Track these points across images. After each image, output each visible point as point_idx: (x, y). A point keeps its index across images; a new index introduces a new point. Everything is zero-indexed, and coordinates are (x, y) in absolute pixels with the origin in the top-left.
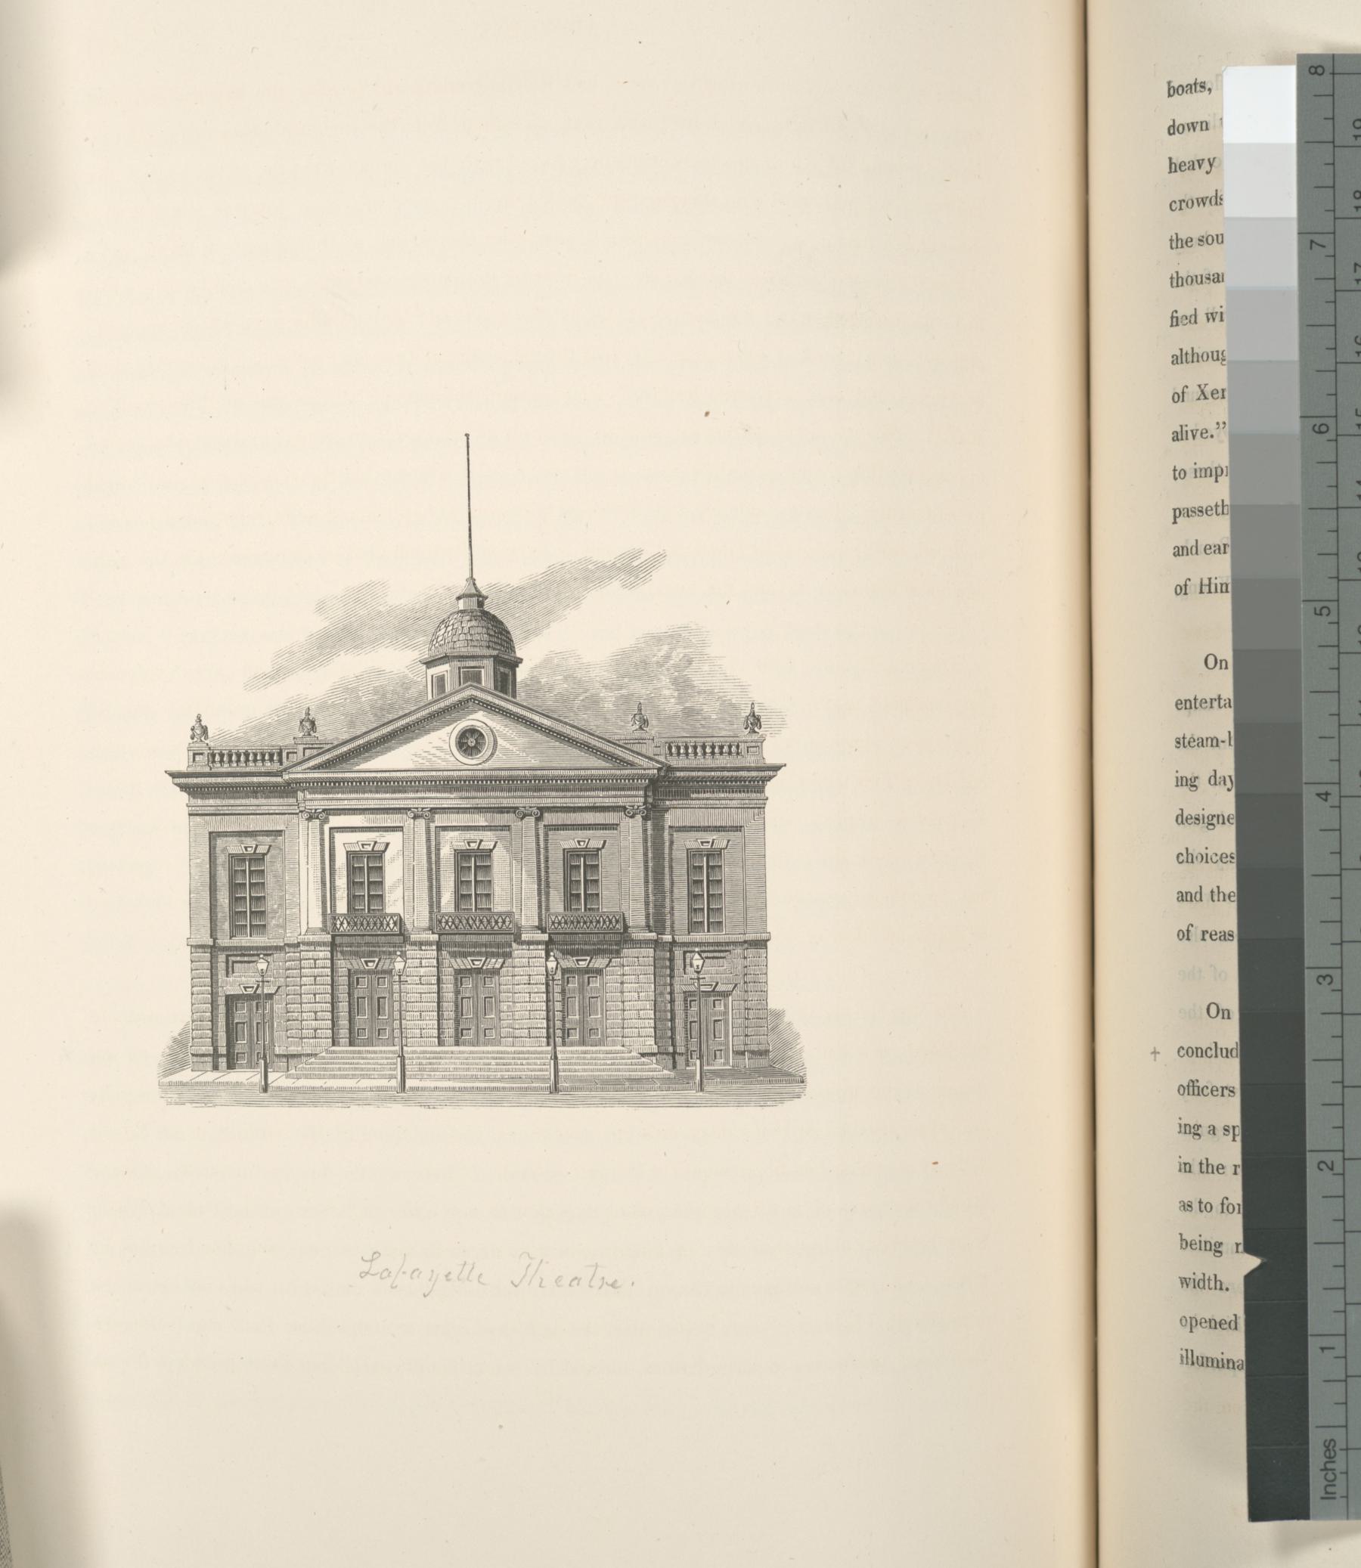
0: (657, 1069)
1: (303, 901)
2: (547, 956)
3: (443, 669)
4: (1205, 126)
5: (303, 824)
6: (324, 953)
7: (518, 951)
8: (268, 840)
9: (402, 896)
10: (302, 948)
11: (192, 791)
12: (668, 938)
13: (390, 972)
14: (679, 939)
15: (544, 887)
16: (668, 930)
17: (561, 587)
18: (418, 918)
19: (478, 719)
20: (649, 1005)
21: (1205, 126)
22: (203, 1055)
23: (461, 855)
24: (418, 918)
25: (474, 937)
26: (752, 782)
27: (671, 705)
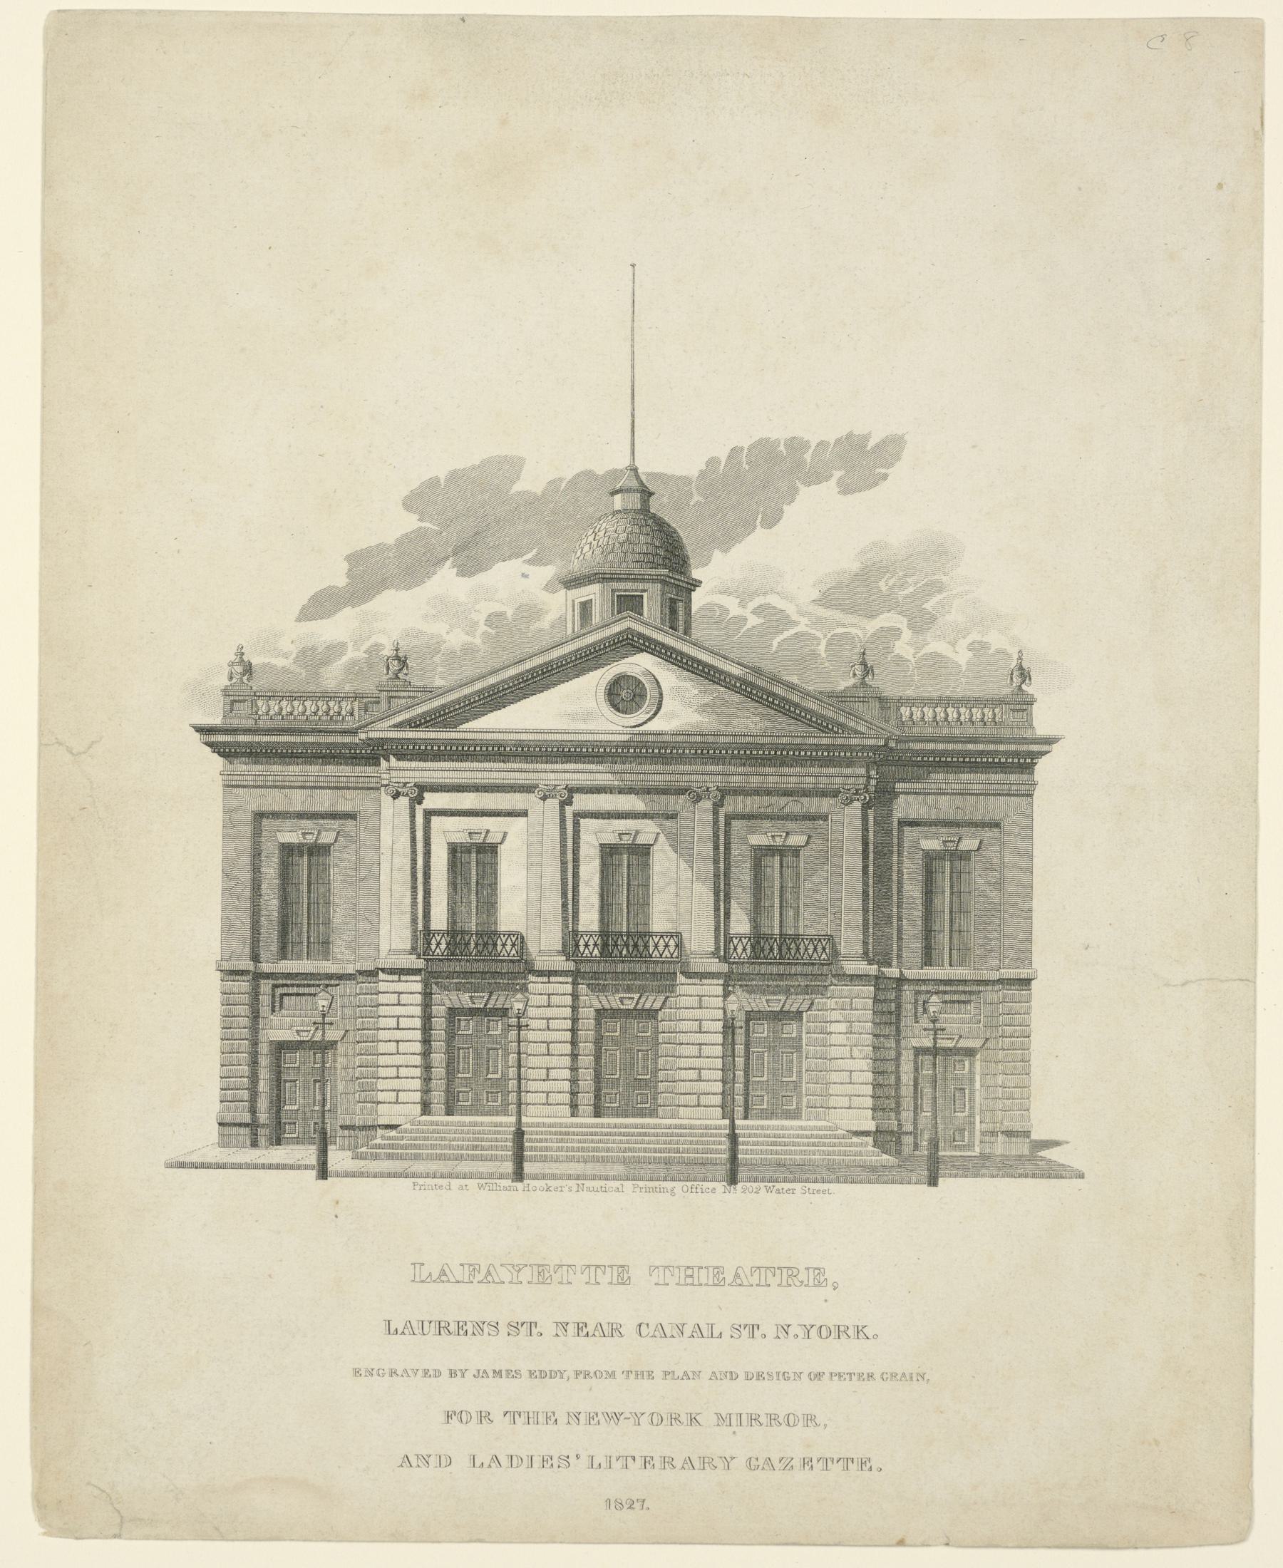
0: (868, 1152)
1: (383, 908)
2: (726, 995)
3: (593, 592)
4: (228, 786)
5: (386, 800)
6: (414, 985)
7: (685, 987)
8: (336, 824)
9: (524, 901)
10: (382, 976)
11: (226, 752)
12: (893, 972)
13: (504, 1012)
14: (909, 974)
15: (722, 895)
16: (895, 962)
17: (762, 480)
18: (546, 944)
19: (640, 664)
20: (865, 1064)
21: (228, 786)
22: (240, 1125)
23: (608, 852)
24: (546, 944)
25: (621, 957)
26: (1018, 761)
27: (963, 657)
